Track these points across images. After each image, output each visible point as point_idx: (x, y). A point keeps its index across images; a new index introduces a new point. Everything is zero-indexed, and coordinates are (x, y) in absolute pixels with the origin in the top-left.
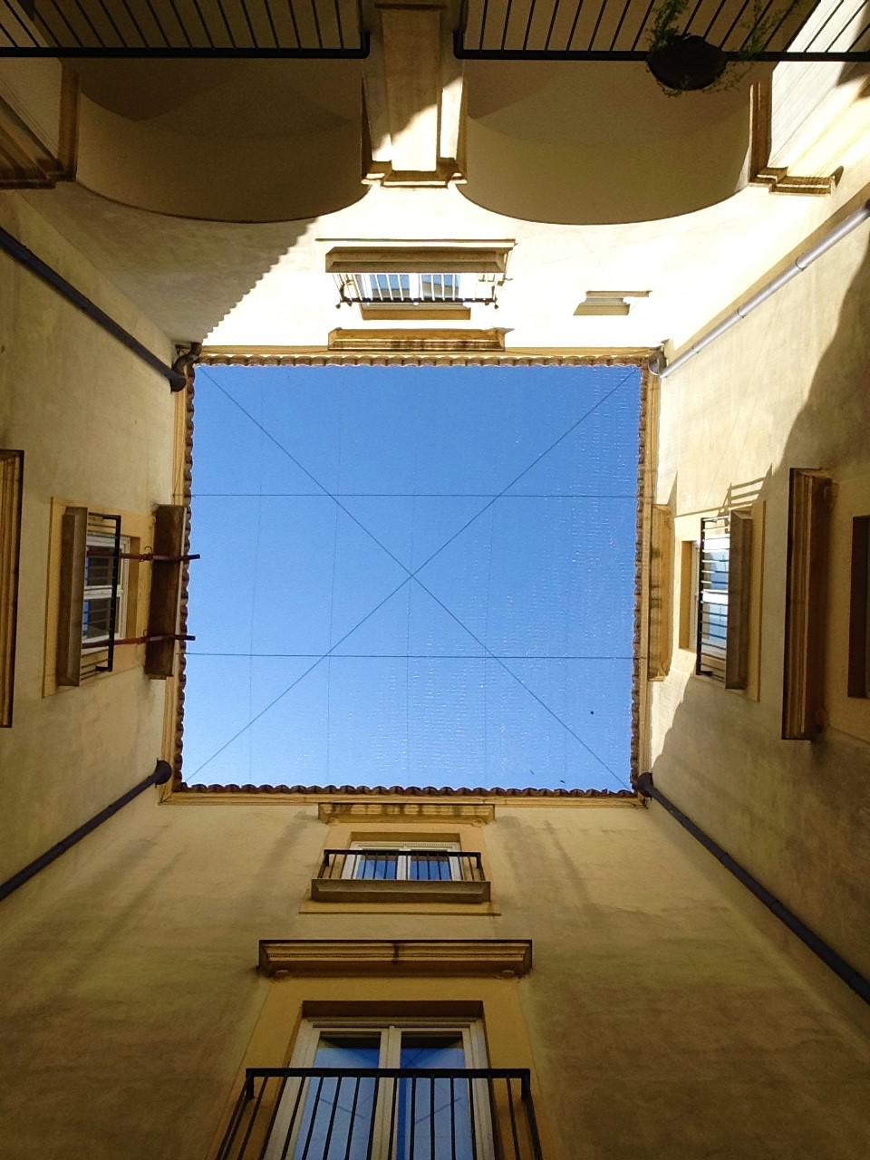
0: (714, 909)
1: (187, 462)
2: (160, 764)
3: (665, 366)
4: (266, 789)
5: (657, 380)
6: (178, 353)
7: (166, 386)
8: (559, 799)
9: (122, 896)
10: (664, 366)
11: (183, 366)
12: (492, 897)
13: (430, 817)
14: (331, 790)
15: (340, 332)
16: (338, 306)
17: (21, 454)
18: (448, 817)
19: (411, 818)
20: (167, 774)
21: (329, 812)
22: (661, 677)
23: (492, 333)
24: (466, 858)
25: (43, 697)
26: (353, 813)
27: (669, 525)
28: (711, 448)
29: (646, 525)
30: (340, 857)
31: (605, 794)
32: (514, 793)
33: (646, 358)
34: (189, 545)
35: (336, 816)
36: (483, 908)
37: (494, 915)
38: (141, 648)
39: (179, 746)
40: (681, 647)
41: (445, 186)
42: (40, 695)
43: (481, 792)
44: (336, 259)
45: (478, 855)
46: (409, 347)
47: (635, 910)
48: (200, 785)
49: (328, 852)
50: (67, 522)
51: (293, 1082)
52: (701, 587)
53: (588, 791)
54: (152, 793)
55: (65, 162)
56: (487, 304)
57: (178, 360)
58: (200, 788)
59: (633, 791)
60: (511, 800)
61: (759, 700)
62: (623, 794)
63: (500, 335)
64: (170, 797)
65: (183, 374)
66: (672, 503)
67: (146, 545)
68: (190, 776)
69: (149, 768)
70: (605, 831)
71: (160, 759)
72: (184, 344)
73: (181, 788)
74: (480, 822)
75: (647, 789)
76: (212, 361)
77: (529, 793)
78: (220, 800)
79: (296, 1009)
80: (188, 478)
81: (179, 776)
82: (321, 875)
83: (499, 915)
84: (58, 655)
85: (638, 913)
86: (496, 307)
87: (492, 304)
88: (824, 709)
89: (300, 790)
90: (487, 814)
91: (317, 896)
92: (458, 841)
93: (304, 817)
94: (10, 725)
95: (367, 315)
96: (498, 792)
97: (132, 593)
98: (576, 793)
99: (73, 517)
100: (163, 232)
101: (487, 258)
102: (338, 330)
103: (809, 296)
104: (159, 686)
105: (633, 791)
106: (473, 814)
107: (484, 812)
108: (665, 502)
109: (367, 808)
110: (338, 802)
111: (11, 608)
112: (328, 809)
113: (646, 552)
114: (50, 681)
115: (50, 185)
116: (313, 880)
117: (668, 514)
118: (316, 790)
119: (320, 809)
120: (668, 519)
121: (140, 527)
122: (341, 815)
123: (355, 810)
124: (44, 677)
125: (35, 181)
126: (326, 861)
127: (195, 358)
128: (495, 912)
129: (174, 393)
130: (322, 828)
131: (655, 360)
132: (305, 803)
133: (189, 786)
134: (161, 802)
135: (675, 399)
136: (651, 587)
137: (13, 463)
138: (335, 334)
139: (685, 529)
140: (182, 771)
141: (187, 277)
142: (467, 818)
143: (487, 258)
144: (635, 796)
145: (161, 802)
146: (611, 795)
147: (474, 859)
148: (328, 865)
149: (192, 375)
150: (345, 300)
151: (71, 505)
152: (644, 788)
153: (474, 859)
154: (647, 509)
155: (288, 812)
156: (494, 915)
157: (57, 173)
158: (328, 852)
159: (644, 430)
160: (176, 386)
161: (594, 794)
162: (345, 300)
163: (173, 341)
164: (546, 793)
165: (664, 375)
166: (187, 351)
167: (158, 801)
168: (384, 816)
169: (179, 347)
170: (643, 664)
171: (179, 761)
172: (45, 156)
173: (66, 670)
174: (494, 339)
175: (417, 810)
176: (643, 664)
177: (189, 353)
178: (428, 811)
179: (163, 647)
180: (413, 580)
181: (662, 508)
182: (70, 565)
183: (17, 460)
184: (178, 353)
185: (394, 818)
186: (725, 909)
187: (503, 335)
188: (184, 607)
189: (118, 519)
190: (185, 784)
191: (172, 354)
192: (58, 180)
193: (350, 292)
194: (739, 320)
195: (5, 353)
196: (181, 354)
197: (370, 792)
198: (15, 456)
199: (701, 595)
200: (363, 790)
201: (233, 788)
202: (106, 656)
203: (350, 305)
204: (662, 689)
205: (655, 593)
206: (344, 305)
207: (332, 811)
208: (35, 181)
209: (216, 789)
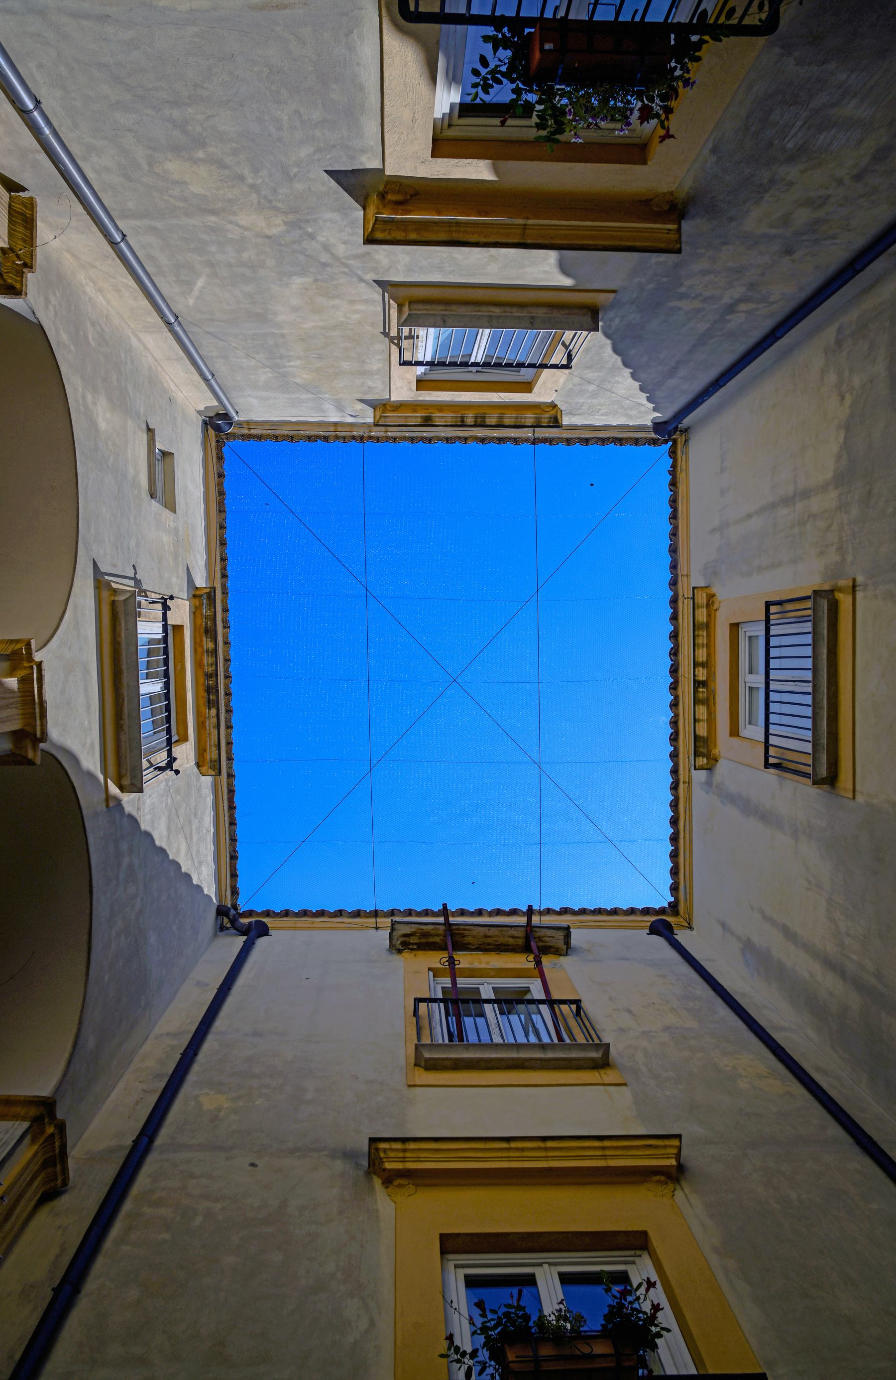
0: (839, 343)
1: (341, 915)
2: (654, 930)
3: (226, 414)
4: (674, 822)
5: (240, 424)
6: (228, 929)
7: (262, 942)
8: (680, 521)
9: (829, 984)
10: (226, 416)
11: (243, 925)
12: (827, 587)
13: (709, 655)
14: (674, 756)
15: (201, 764)
16: (177, 772)
17: (373, 1141)
18: (708, 635)
19: (711, 674)
20: (662, 924)
21: (705, 760)
22: (559, 412)
23: (197, 601)
24: (772, 617)
25: (625, 1085)
26: (705, 735)
27: (399, 406)
28: (320, 357)
29: (393, 432)
30: (772, 751)
31: (673, 472)
32: (674, 567)
33: (216, 436)
34: (426, 910)
35: (709, 752)
36: (845, 600)
37: (854, 586)
38: (546, 961)
39: (632, 911)
40: (530, 391)
41: (39, 665)
42: (624, 1088)
43: (674, 601)
44: (126, 782)
45: (768, 605)
46: (211, 690)
47: (842, 434)
48: (671, 889)
49: (767, 765)
50: (432, 1066)
51: (773, 740)
52: (465, 364)
53: (671, 490)
54: (682, 936)
55: (33, 1111)
56: (169, 609)
57: (235, 929)
58: (674, 889)
59: (670, 443)
60: (682, 569)
61: (614, 291)
62: (673, 453)
63: (198, 593)
64: (685, 920)
65: (250, 923)
66: (374, 405)
67: (437, 959)
68: (661, 899)
69: (658, 941)
70: (722, 471)
71: (648, 931)
72: (219, 923)
73: (674, 907)
74: (713, 602)
75: (671, 428)
76: (235, 892)
77: (673, 550)
78: (687, 868)
79: (735, 740)
80: (358, 914)
81: (662, 911)
82: (805, 775)
83: (854, 580)
84: (579, 1068)
85: (847, 428)
86: (172, 598)
87: (169, 602)
88: (651, 200)
89: (675, 787)
90: (704, 595)
91: (829, 780)
92: (737, 625)
93: (709, 783)
94: (679, 1137)
95: (184, 738)
96: (674, 583)
97: (488, 974)
98: (673, 502)
99: (427, 1060)
100: (107, 977)
101: (117, 614)
102: (198, 765)
103: (155, 229)
104: (577, 937)
105: (670, 443)
106: (705, 609)
107: (701, 598)
108: (370, 411)
109: (699, 721)
110: (694, 750)
111: (550, 1144)
112: (702, 761)
113: (426, 432)
114: (609, 1076)
115: (61, 1127)
116: (813, 784)
117: (382, 406)
118: (675, 771)
119: (702, 768)
120: (391, 406)
121: (420, 973)
122: (708, 746)
123: (702, 731)
124: (604, 1085)
125: (57, 1144)
126: (777, 766)
127: (233, 912)
128: (851, 584)
129: (271, 932)
130: (722, 767)
131: (217, 425)
132: (689, 783)
133: (672, 899)
134: (690, 928)
135: (257, 406)
136: (463, 424)
137: (385, 1150)
138: (204, 769)
139: (402, 387)
140: (657, 907)
141: (152, 939)
142: (709, 615)
143: (117, 614)
144: (675, 442)
145: (690, 928)
146: (674, 466)
147: (773, 609)
148: (780, 764)
149: (250, 913)
150: (169, 766)
151: (412, 1061)
152: (669, 432)
153: (773, 609)
154: (378, 432)
155: (700, 799)
156: (854, 586)
157: (46, 1120)
158: (767, 765)
159: (292, 437)
160: (263, 931)
161: (673, 484)
162: (169, 766)
163: (215, 935)
164: (674, 534)
165: (234, 415)
166: (226, 920)
167: (688, 931)
168: (708, 702)
169: (222, 928)
170: (541, 433)
171: (646, 911)
172: (28, 1139)
173: (593, 1059)
174: (203, 599)
175: (701, 669)
176: (541, 433)
177: (228, 917)
178: (702, 655)
179: (537, 938)
180: (459, 680)
181: (379, 413)
182: (479, 1060)
183: (382, 1145)
184: (228, 929)
185: (712, 695)
186: (840, 330)
187: (197, 588)
188: (491, 913)
189: (418, 1001)
190: (670, 904)
191: (228, 935)
192: (55, 1118)
193: (161, 758)
194: (180, 324)
195: (256, 1162)
196: (229, 925)
197: (676, 716)
198: (377, 1149)
199: (475, 364)
200: (674, 723)
201: (674, 855)
202: (565, 1008)
203: (175, 759)
204: (571, 414)
205: (470, 421)
206: (175, 766)
207: (703, 756)
208: (57, 1144)
209: (674, 872)
